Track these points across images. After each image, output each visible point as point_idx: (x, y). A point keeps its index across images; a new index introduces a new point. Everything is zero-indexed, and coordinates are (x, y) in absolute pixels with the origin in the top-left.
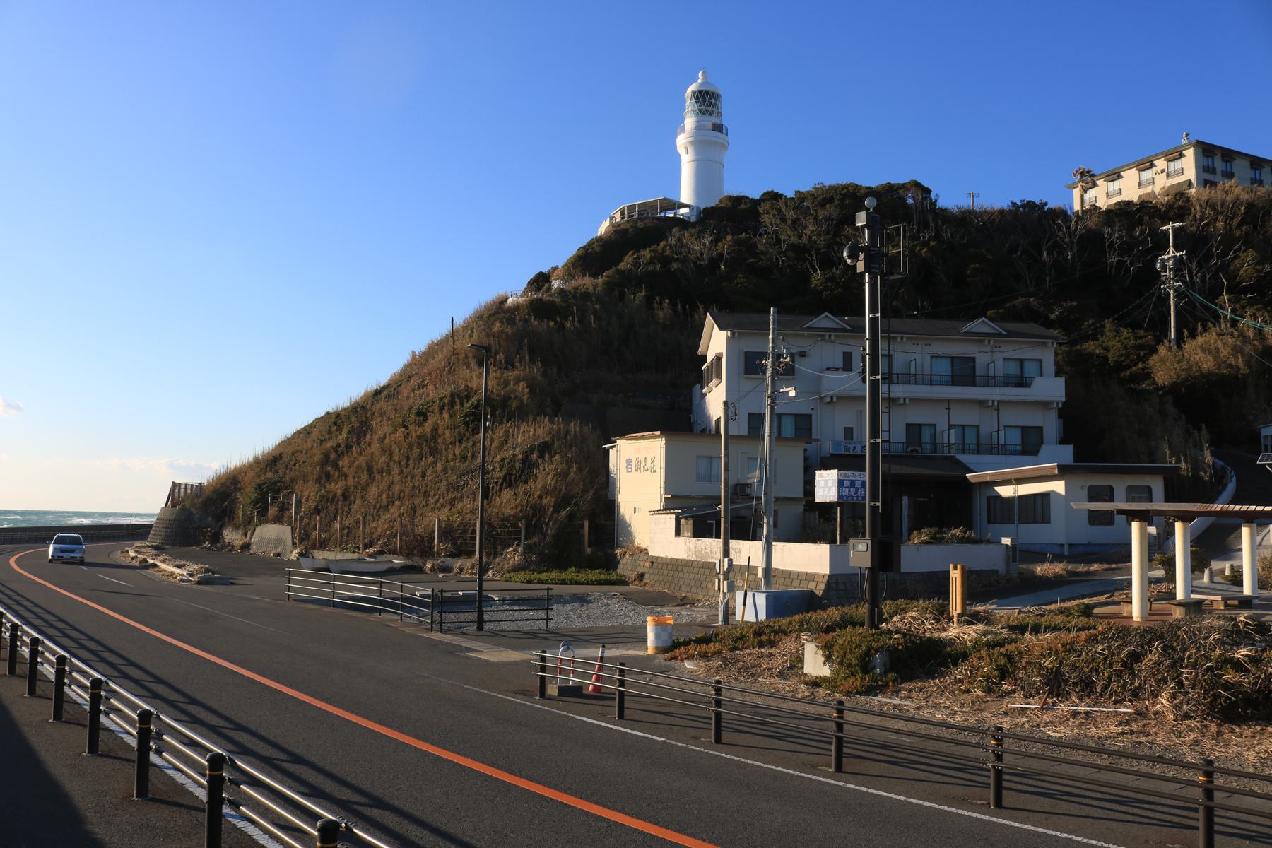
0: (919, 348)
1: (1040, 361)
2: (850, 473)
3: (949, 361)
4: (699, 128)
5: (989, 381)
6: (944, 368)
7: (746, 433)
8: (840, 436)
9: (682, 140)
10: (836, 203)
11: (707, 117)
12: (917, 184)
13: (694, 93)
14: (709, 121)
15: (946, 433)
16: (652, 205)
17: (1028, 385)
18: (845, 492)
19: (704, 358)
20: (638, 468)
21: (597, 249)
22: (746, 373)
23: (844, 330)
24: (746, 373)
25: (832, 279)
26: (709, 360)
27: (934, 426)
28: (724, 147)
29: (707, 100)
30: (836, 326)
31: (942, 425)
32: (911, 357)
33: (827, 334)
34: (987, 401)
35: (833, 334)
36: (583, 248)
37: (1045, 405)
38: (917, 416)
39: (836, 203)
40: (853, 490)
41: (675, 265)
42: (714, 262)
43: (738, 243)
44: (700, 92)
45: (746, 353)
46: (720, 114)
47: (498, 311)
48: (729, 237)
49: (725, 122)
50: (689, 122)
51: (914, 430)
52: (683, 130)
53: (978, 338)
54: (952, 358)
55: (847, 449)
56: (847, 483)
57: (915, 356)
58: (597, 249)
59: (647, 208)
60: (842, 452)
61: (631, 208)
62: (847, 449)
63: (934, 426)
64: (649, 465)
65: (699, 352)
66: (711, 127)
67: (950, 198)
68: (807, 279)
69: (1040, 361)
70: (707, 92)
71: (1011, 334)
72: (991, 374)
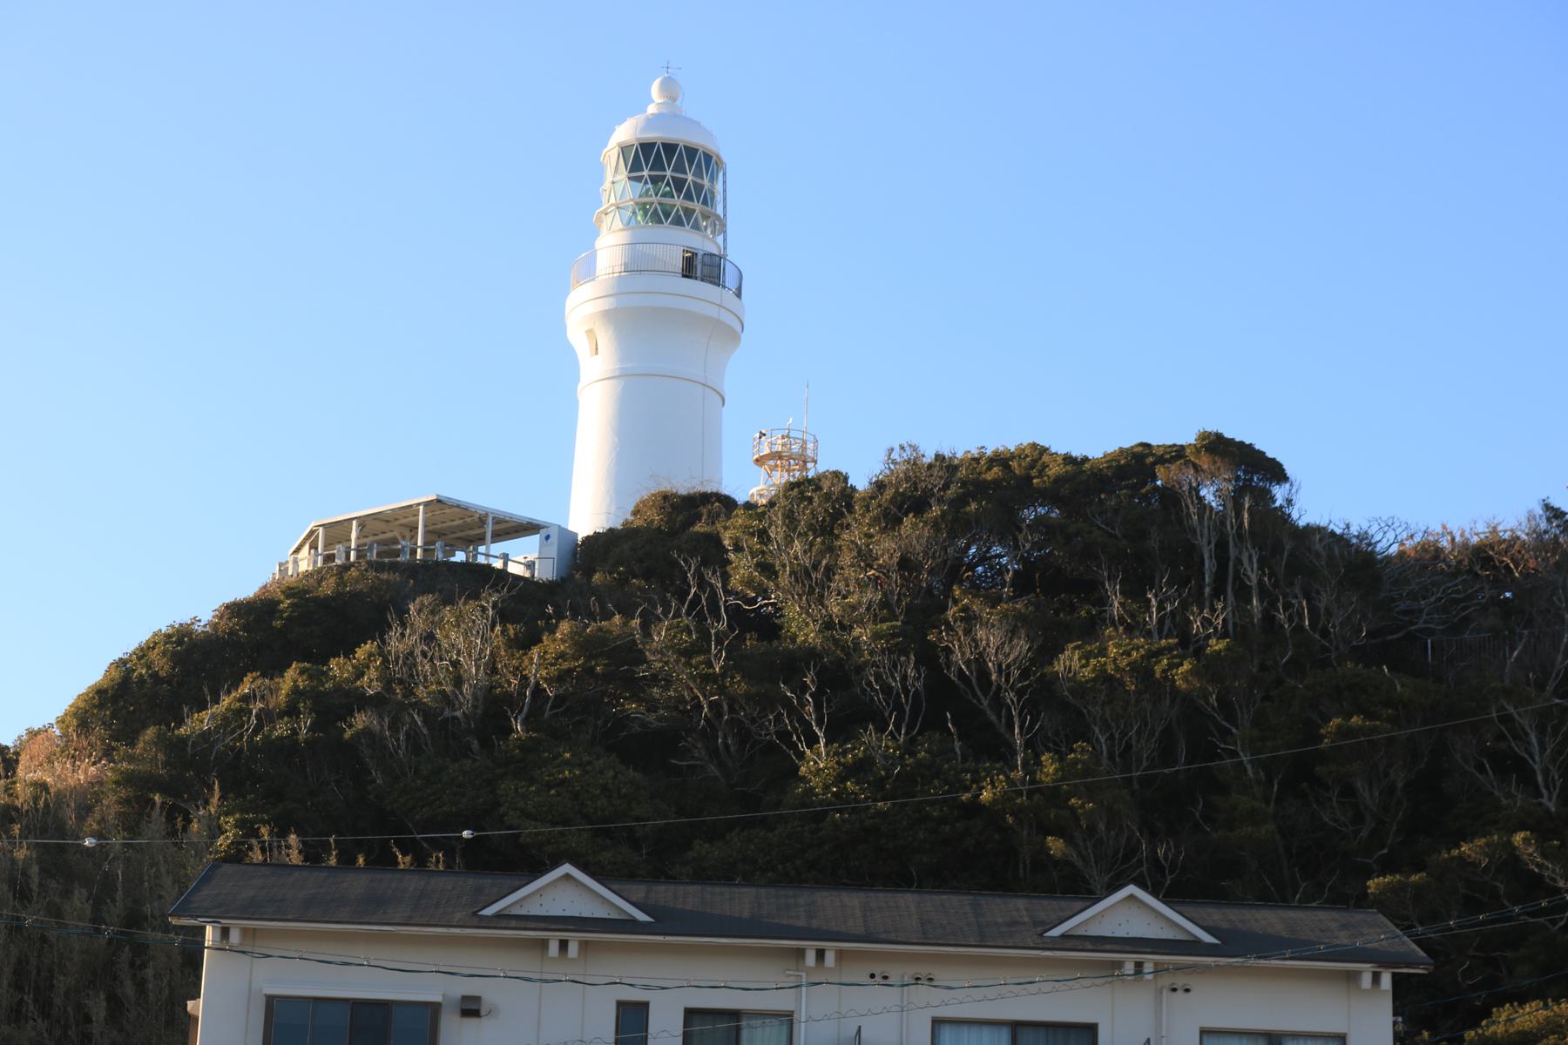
1: (937, 1023)
3: (1004, 1036)
4: (635, 267)
9: (583, 309)
10: (936, 511)
11: (667, 231)
12: (1217, 446)
13: (624, 149)
14: (675, 242)
16: (401, 519)
21: (162, 665)
23: (630, 925)
25: (859, 769)
28: (730, 334)
29: (672, 172)
30: (600, 912)
33: (553, 939)
35: (575, 939)
36: (122, 662)
39: (936, 511)
41: (361, 720)
42: (495, 706)
43: (586, 646)
44: (646, 147)
45: (271, 1001)
46: (720, 225)
48: (565, 627)
49: (740, 245)
50: (610, 246)
52: (589, 273)
53: (1110, 956)
58: (162, 665)
59: (384, 529)
61: (337, 531)
66: (678, 264)
67: (1314, 501)
68: (780, 766)
69: (937, 1023)
70: (670, 148)
71: (1232, 944)
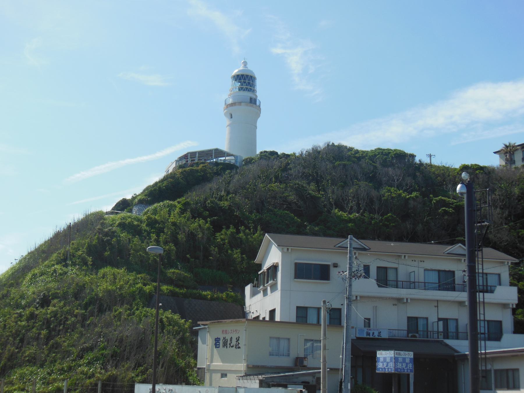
0: (416, 264)
2: (402, 352)
5: (411, 284)
6: (434, 278)
7: (295, 321)
8: (361, 324)
15: (436, 324)
17: (492, 292)
18: (399, 366)
19: (260, 266)
20: (225, 345)
22: (295, 278)
24: (295, 278)
26: (265, 268)
27: (427, 319)
30: (358, 247)
31: (433, 318)
32: (411, 269)
34: (403, 299)
37: (505, 306)
38: (414, 311)
40: (385, 364)
45: (296, 264)
47: (92, 222)
51: (413, 321)
54: (439, 271)
55: (368, 334)
56: (400, 360)
57: (416, 269)
60: (365, 336)
62: (368, 334)
63: (427, 319)
64: (234, 342)
65: (257, 261)
72: (412, 280)
